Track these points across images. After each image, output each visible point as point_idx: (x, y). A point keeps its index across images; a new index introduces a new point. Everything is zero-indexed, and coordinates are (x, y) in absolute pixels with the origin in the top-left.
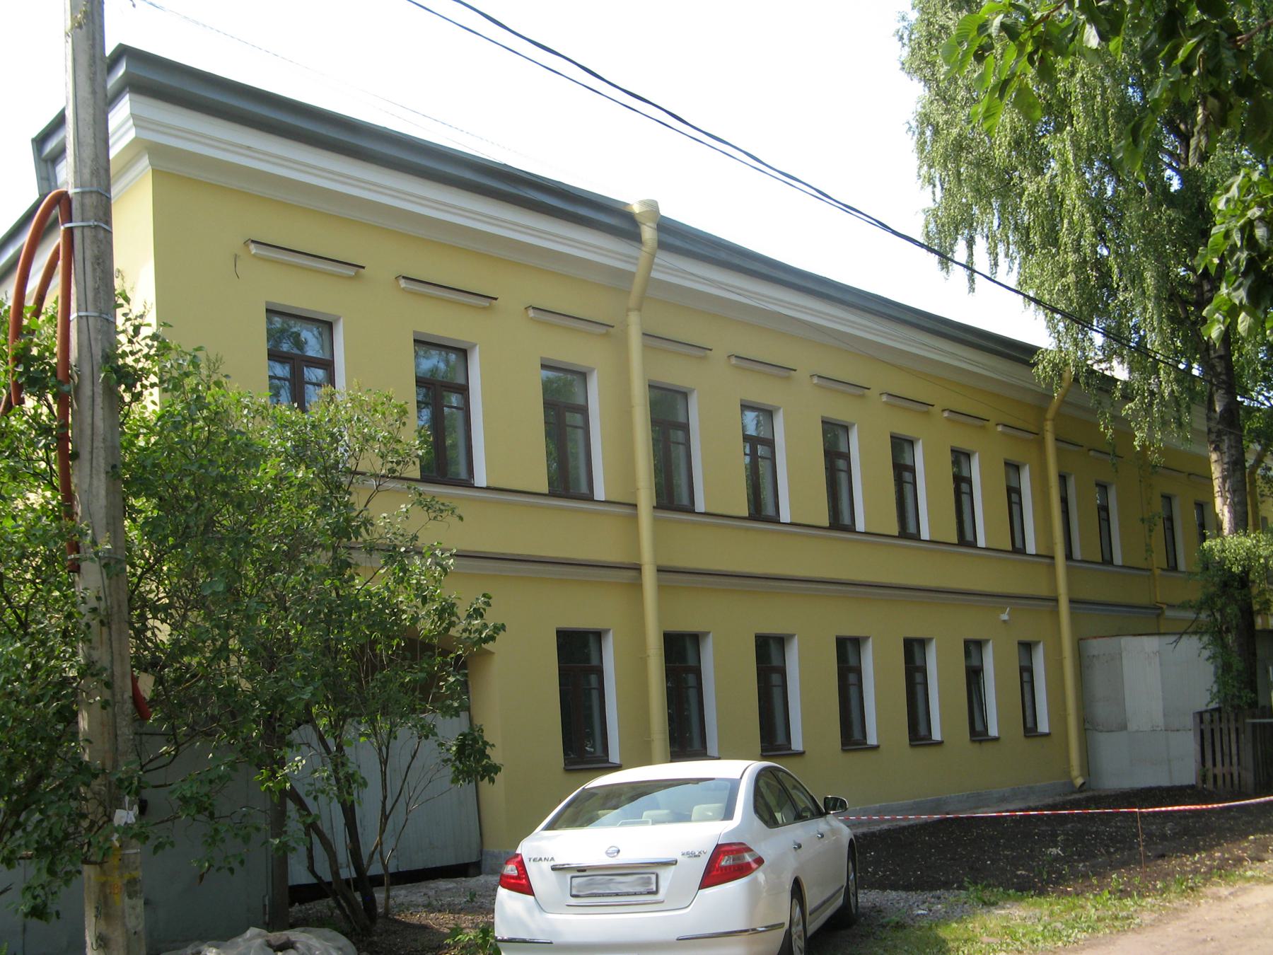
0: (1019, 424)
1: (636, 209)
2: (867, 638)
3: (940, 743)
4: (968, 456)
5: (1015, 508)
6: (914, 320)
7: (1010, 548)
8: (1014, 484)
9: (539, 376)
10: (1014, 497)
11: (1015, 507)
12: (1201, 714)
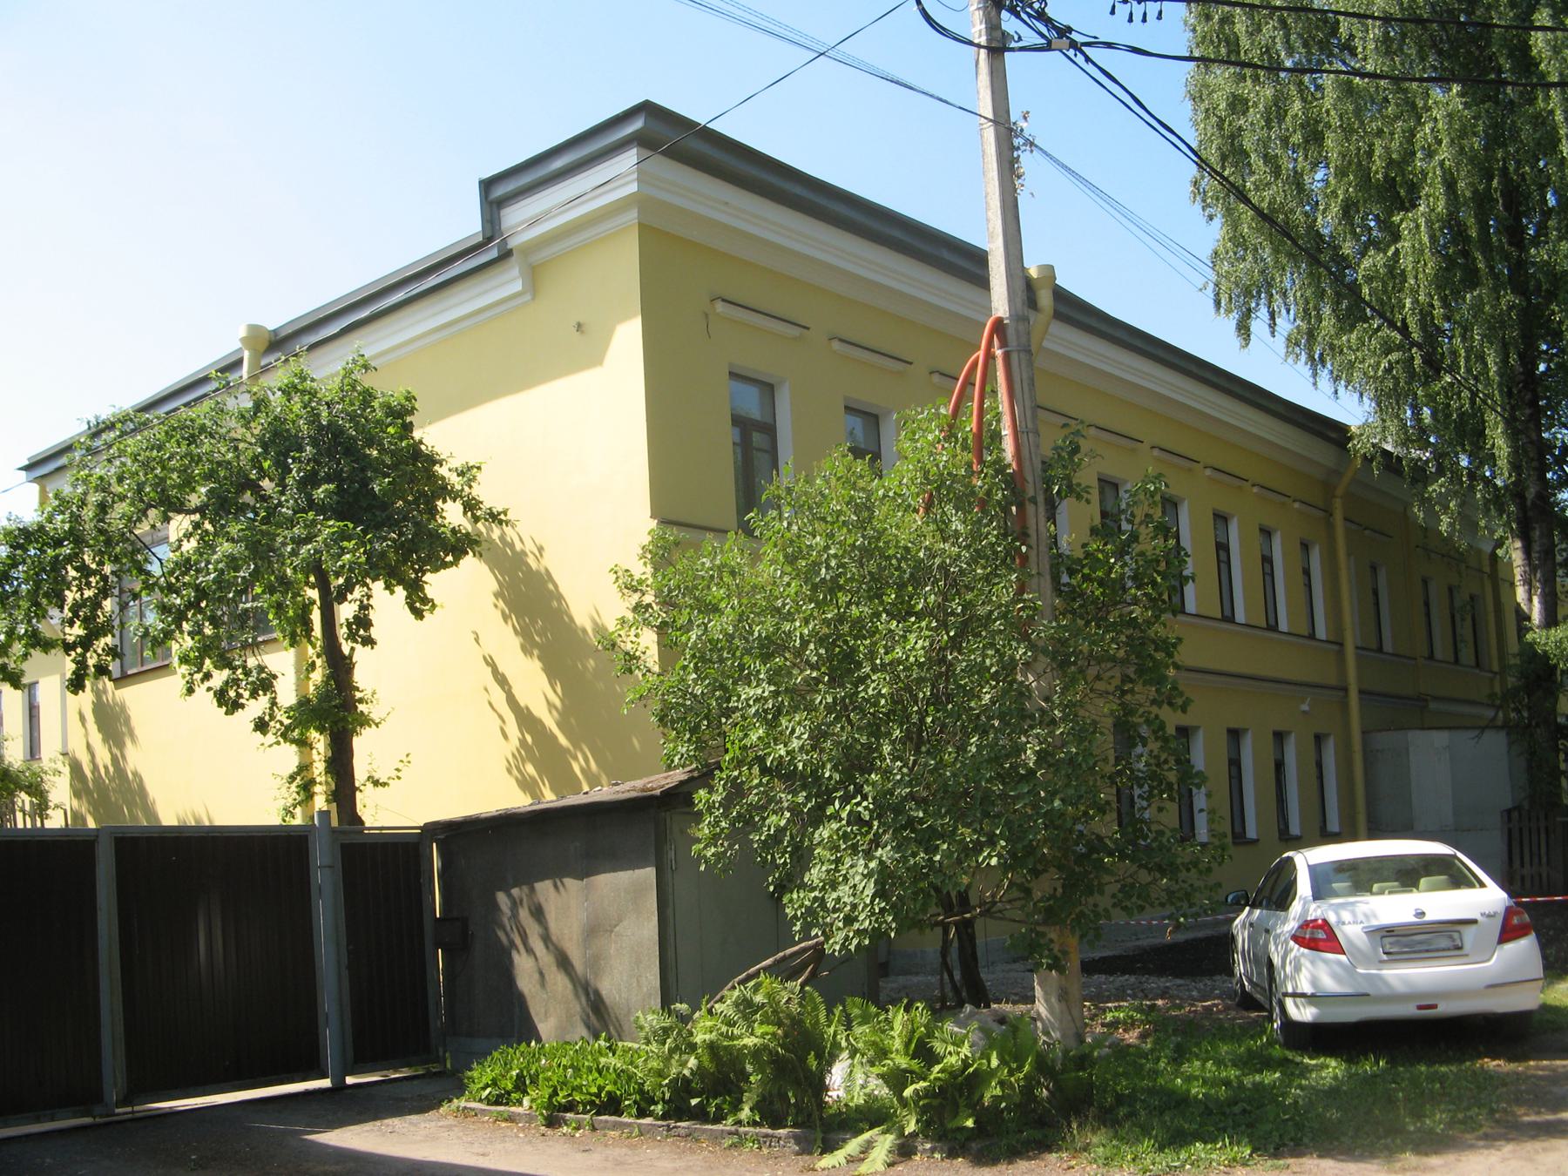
0: (1267, 485)
2: (1197, 728)
3: (1255, 841)
8: (1222, 540)
10: (1223, 555)
12: (1509, 812)
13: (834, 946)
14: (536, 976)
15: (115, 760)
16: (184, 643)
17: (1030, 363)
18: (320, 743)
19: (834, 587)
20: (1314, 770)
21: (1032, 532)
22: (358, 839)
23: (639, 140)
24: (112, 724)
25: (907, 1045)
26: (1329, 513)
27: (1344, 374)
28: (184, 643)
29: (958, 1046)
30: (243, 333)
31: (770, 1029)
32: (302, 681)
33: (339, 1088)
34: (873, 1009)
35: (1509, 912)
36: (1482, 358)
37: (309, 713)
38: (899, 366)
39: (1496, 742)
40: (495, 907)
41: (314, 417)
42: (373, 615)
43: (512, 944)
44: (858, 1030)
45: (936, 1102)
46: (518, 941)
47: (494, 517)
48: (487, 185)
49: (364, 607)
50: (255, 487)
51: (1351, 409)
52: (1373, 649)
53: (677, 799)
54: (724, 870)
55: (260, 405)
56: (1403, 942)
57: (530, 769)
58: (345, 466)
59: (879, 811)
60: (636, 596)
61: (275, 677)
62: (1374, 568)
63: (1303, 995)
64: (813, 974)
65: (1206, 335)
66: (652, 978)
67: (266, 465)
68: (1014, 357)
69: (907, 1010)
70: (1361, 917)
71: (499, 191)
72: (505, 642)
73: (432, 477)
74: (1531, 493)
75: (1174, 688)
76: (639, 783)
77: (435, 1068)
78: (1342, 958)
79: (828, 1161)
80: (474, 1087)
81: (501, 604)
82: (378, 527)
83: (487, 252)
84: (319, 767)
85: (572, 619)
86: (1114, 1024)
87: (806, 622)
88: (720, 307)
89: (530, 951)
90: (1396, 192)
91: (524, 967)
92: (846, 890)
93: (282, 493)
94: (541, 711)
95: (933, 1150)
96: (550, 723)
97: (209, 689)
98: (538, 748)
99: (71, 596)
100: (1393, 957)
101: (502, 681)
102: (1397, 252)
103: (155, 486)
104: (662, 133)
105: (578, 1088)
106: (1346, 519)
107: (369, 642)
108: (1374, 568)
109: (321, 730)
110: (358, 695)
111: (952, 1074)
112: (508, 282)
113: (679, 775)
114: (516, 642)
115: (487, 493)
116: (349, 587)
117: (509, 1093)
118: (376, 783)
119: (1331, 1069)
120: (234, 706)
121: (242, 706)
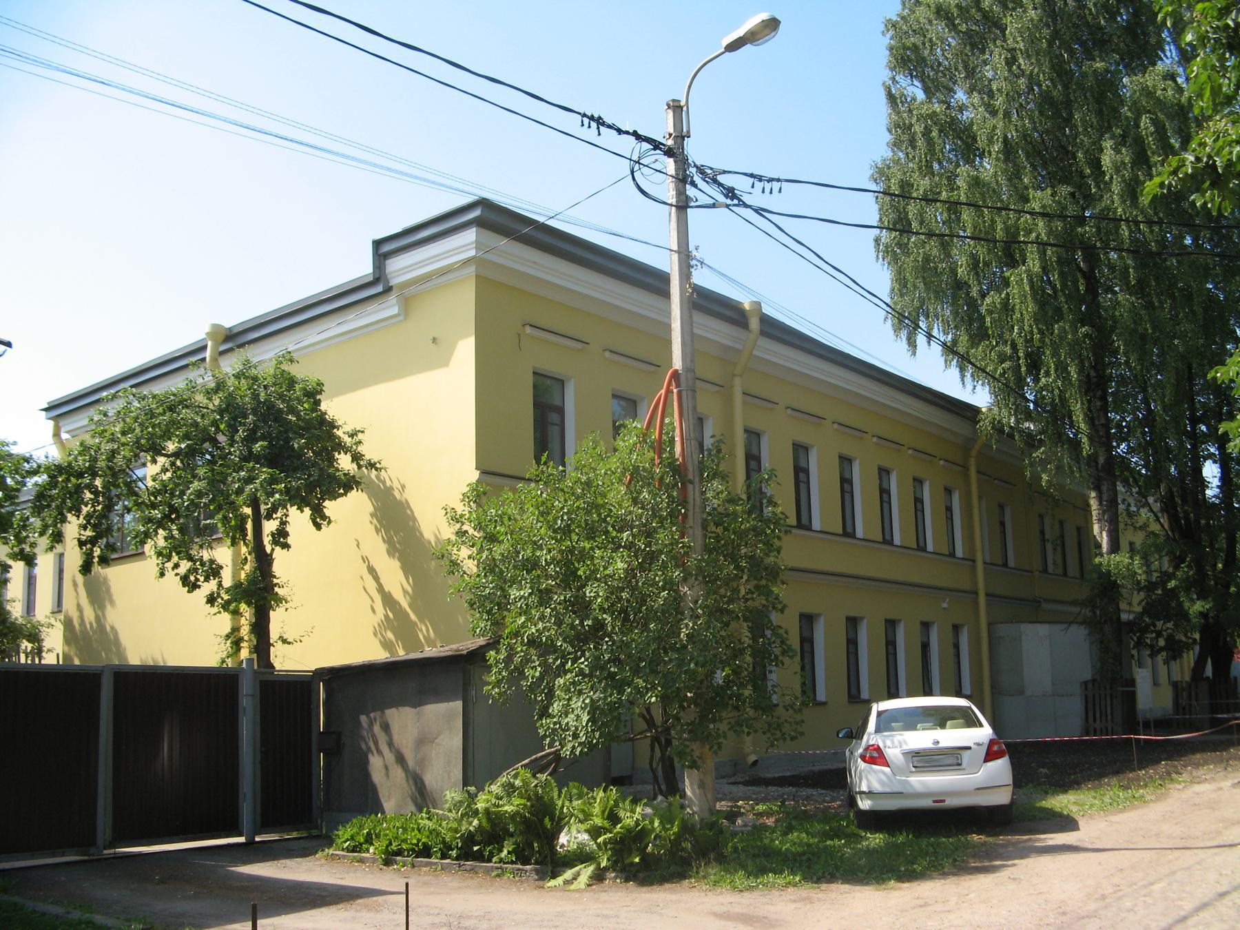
1: (747, 307)
2: (819, 615)
4: (888, 472)
5: (847, 496)
6: (879, 376)
7: (841, 532)
9: (529, 380)
11: (803, 486)
12: (1086, 683)
13: (566, 752)
14: (384, 771)
15: (97, 618)
16: (160, 539)
17: (694, 398)
18: (247, 611)
19: (567, 531)
20: (951, 650)
21: (690, 500)
22: (270, 678)
23: (478, 222)
24: (98, 595)
25: (603, 812)
26: (966, 468)
27: (981, 372)
28: (160, 539)
29: (632, 816)
30: (207, 329)
31: (523, 801)
32: (235, 574)
33: (250, 844)
34: (586, 790)
35: (992, 742)
36: (1065, 369)
37: (241, 592)
38: (652, 368)
39: (1079, 633)
40: (359, 723)
41: (255, 396)
42: (288, 529)
43: (369, 749)
44: (575, 803)
45: (617, 847)
46: (373, 748)
47: (372, 465)
48: (377, 244)
49: (283, 523)
50: (214, 441)
51: (980, 397)
52: (999, 564)
53: (476, 657)
54: (504, 704)
55: (220, 386)
56: (925, 760)
57: (390, 635)
58: (275, 428)
59: (593, 668)
60: (458, 526)
61: (221, 567)
62: (1001, 507)
63: (864, 793)
64: (555, 770)
65: (882, 346)
66: (458, 773)
67: (222, 427)
68: (684, 393)
69: (605, 791)
70: (896, 743)
71: (386, 248)
72: (376, 547)
73: (332, 437)
74: (1101, 460)
75: (777, 598)
76: (454, 647)
77: (315, 832)
78: (886, 769)
79: (552, 883)
80: (339, 841)
81: (375, 521)
82: (295, 470)
83: (375, 286)
84: (245, 631)
85: (421, 534)
86: (760, 815)
87: (549, 551)
88: (528, 330)
89: (379, 752)
90: (1011, 254)
91: (375, 763)
92: (572, 716)
93: (232, 446)
94: (399, 596)
95: (616, 878)
96: (404, 603)
97: (177, 574)
98: (397, 622)
99: (85, 510)
100: (919, 769)
101: (371, 570)
102: (1008, 294)
103: (148, 440)
104: (493, 218)
105: (405, 841)
106: (978, 472)
107: (286, 546)
108: (1001, 507)
109: (249, 604)
110: (275, 581)
111: (629, 830)
112: (389, 308)
113: (481, 641)
114: (383, 547)
115: (369, 451)
116: (274, 509)
117: (361, 844)
118: (285, 641)
119: (875, 840)
120: (194, 587)
121: (199, 587)
